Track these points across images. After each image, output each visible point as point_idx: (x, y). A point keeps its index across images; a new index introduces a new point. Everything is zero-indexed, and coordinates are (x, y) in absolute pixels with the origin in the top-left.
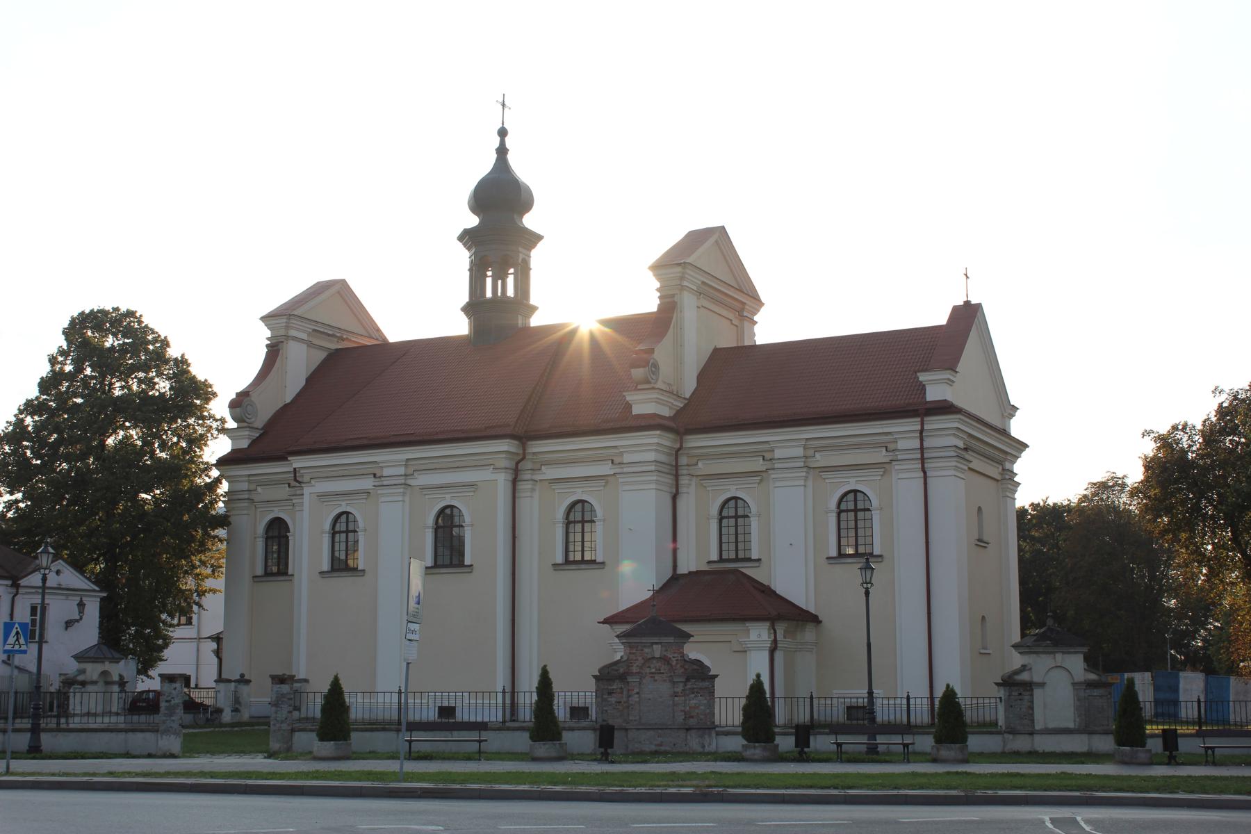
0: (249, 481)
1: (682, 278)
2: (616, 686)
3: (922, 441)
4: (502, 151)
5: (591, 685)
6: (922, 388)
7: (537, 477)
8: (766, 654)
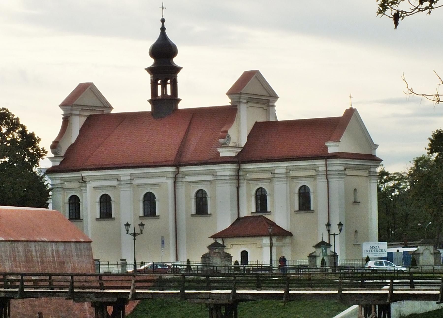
0: (61, 180)
1: (240, 98)
2: (207, 259)
3: (238, 173)
4: (163, 29)
5: (200, 259)
6: (326, 148)
7: (184, 180)
8: (269, 248)
